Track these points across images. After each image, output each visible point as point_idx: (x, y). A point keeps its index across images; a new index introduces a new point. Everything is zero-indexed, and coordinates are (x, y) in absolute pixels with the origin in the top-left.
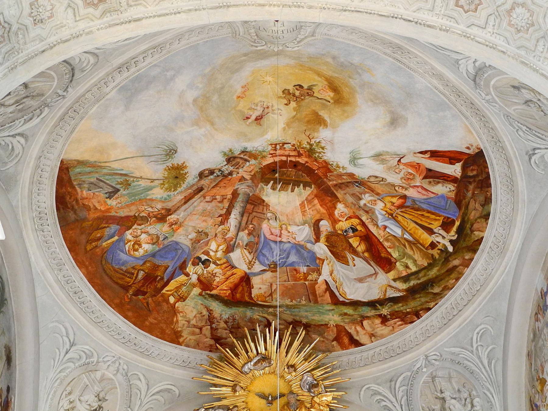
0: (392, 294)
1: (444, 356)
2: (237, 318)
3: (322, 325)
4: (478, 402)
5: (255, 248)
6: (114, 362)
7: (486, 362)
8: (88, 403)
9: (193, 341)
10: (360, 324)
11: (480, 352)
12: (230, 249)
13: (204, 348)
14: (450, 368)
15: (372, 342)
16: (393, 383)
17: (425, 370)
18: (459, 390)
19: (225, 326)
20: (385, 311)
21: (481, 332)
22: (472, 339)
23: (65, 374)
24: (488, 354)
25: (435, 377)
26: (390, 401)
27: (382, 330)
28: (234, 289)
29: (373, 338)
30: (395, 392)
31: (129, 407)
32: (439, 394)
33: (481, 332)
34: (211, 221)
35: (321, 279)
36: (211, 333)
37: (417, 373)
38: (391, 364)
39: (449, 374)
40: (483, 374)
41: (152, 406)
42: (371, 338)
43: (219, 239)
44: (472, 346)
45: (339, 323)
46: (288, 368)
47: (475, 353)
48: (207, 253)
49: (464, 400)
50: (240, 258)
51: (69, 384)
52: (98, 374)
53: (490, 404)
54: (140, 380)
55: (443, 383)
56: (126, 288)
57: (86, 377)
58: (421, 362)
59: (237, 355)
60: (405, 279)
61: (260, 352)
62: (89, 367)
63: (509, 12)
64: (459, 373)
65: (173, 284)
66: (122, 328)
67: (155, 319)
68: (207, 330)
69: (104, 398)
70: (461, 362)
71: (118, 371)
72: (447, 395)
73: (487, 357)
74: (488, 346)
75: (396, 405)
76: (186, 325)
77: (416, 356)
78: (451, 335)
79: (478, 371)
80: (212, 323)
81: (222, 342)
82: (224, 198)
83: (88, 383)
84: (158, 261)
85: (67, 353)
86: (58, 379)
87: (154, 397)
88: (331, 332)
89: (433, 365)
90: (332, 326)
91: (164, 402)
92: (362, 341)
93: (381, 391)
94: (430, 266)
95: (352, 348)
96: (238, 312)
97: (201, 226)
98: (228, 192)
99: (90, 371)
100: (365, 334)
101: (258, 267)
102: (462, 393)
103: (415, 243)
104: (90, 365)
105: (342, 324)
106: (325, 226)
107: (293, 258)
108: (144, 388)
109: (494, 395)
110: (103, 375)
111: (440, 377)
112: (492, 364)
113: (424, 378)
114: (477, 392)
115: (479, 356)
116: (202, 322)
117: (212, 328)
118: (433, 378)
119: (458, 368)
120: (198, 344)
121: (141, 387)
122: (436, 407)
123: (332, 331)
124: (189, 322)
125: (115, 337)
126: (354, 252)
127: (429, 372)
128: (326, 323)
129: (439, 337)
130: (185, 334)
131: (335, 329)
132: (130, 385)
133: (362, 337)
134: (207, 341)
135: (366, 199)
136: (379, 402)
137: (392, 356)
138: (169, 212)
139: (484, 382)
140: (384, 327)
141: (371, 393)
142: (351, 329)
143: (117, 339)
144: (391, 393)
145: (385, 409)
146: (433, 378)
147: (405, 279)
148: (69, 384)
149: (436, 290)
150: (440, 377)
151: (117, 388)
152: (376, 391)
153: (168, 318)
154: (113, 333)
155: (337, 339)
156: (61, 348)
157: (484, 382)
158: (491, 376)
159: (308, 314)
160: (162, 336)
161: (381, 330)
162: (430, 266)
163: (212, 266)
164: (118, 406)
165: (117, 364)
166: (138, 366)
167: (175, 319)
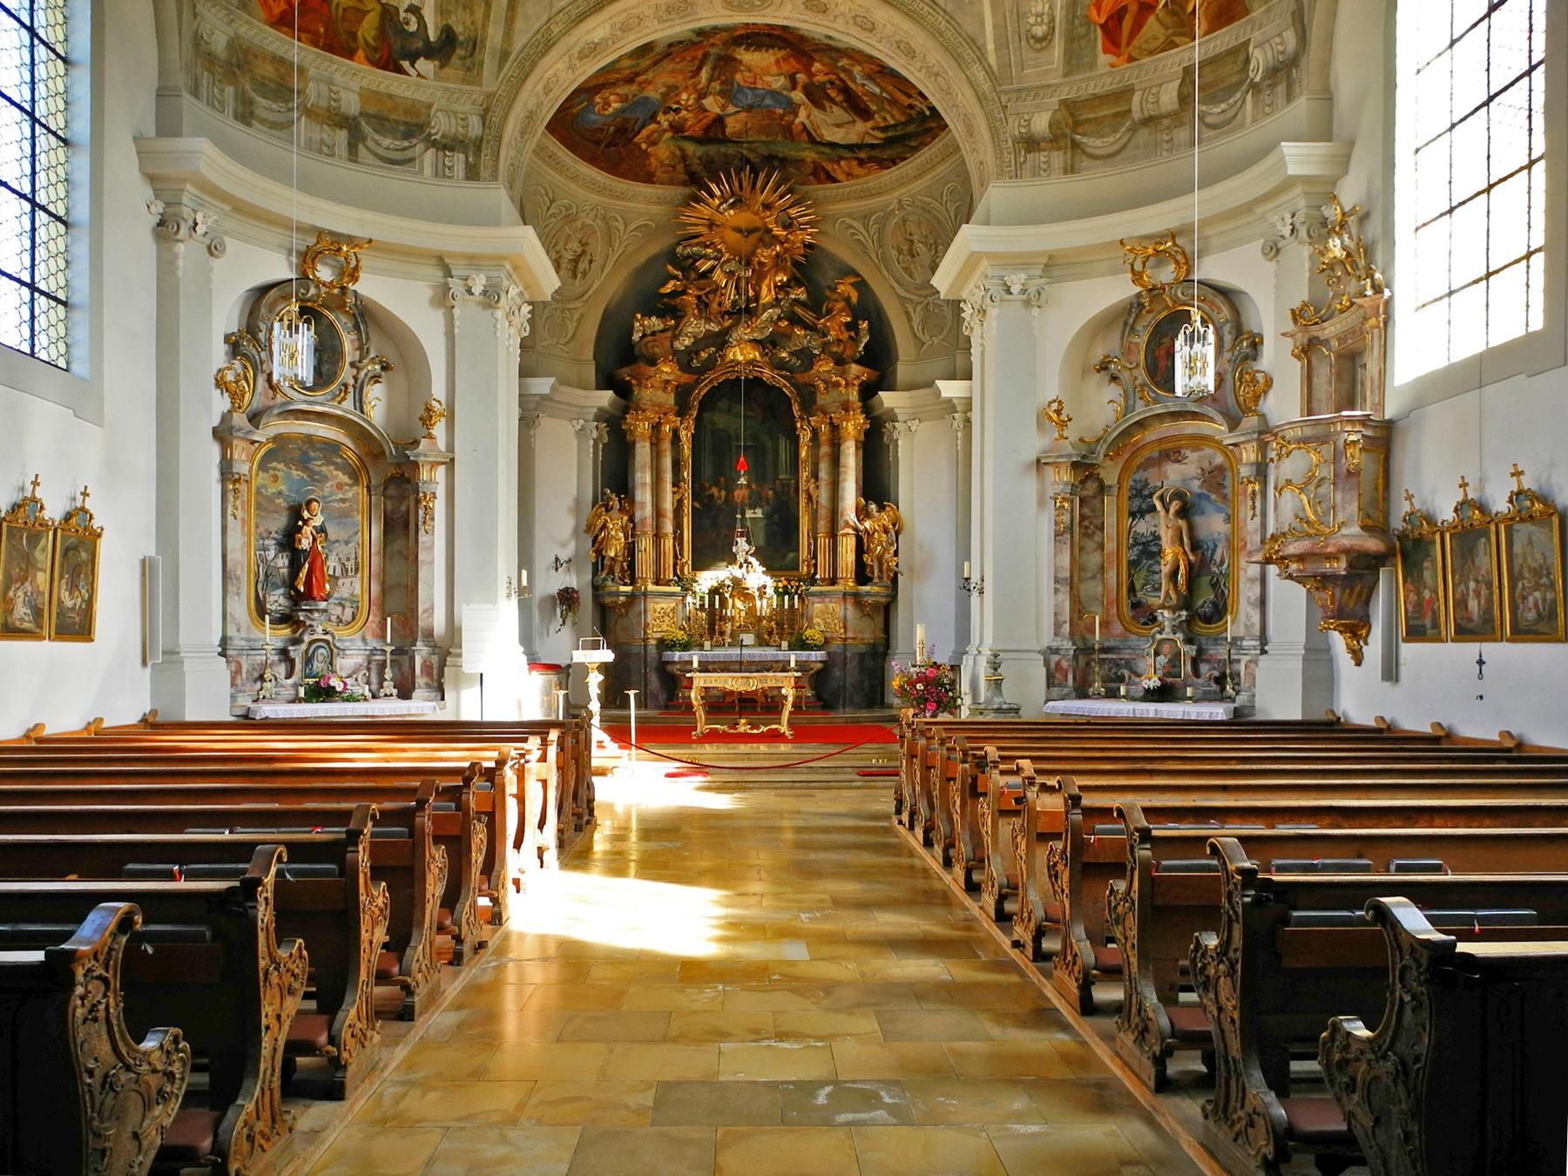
0: (869, 140)
5: (729, 93)
12: (702, 95)
20: (862, 155)
28: (707, 129)
34: (680, 77)
35: (797, 121)
43: (691, 89)
48: (678, 103)
50: (712, 104)
52: (579, 224)
56: (598, 143)
60: (884, 129)
62: (569, 219)
65: (644, 133)
68: (680, 167)
72: (915, 237)
77: (890, 198)
81: (695, 180)
82: (694, 58)
84: (627, 115)
94: (907, 123)
96: (712, 149)
97: (670, 81)
98: (700, 54)
101: (731, 109)
103: (894, 102)
106: (801, 77)
107: (768, 101)
108: (621, 227)
126: (832, 101)
130: (658, 174)
133: (840, 176)
135: (843, 62)
136: (852, 235)
138: (637, 74)
142: (829, 167)
147: (884, 129)
149: (913, 143)
155: (815, 173)
159: (784, 150)
160: (636, 178)
161: (858, 170)
162: (907, 123)
163: (684, 113)
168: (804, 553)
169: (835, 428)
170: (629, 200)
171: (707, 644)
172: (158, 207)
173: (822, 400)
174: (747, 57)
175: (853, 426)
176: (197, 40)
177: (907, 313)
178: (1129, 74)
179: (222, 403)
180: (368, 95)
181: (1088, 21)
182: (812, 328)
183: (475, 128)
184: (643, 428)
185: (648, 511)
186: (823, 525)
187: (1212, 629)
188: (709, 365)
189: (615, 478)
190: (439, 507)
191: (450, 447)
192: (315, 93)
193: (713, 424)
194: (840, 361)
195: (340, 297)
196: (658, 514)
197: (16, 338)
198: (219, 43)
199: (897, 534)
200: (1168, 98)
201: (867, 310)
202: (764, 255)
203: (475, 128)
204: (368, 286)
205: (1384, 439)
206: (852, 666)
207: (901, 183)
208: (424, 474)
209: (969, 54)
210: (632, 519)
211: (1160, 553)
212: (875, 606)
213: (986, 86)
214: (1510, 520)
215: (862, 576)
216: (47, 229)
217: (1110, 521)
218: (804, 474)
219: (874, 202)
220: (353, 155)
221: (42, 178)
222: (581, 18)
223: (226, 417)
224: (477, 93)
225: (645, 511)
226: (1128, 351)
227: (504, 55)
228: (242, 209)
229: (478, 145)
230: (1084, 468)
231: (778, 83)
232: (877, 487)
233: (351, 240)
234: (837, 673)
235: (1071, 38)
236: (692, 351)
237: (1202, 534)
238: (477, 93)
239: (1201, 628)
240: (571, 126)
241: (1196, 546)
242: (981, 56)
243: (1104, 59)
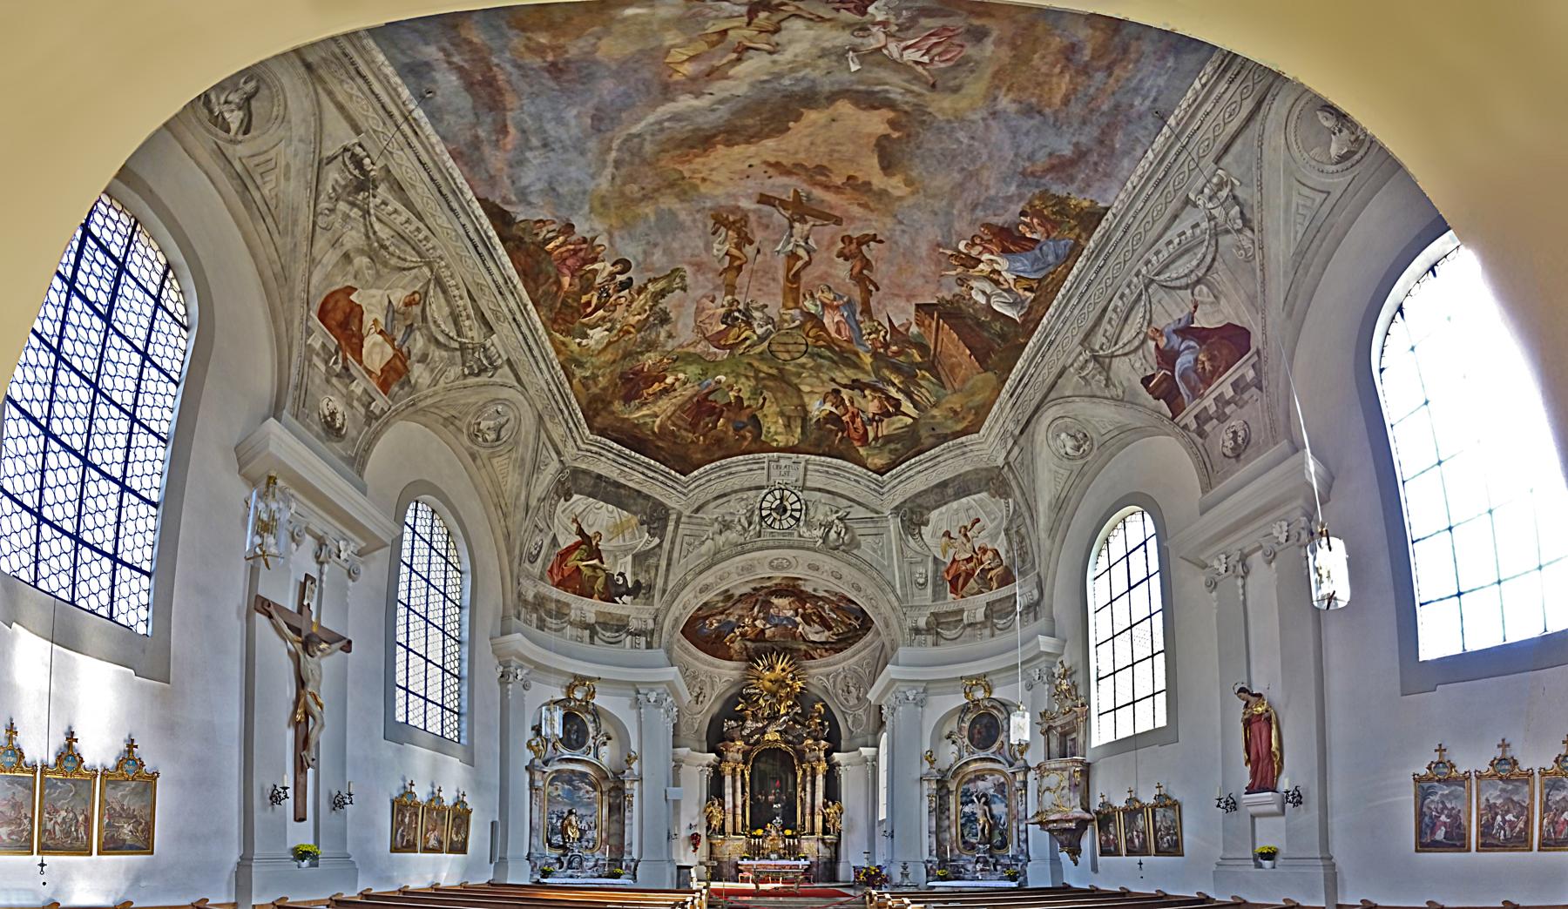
5: (766, 619)
63: (560, 847)
81: (751, 658)
103: (843, 622)
169: (813, 769)
172: (501, 669)
173: (808, 755)
174: (775, 601)
175: (822, 768)
176: (520, 594)
178: (961, 603)
179: (529, 755)
180: (598, 613)
181: (943, 578)
182: (803, 725)
183: (651, 625)
184: (728, 770)
186: (808, 811)
187: (1002, 852)
188: (758, 742)
189: (716, 789)
190: (635, 800)
191: (641, 774)
192: (574, 615)
194: (816, 739)
195: (585, 706)
196: (735, 806)
197: (19, 562)
198: (530, 597)
200: (980, 616)
201: (828, 715)
202: (783, 693)
203: (651, 625)
204: (598, 701)
205: (1087, 770)
207: (844, 660)
208: (627, 786)
209: (888, 589)
211: (977, 820)
213: (896, 604)
214: (1154, 808)
215: (826, 831)
216: (451, 681)
217: (952, 807)
220: (592, 642)
221: (448, 658)
222: (701, 573)
223: (532, 761)
224: (651, 609)
225: (729, 806)
226: (960, 729)
227: (664, 591)
228: (539, 667)
229: (652, 632)
230: (942, 783)
231: (790, 613)
233: (591, 679)
235: (935, 585)
236: (751, 735)
237: (995, 812)
238: (651, 609)
239: (997, 852)
240: (692, 630)
241: (993, 817)
242: (894, 591)
243: (950, 596)
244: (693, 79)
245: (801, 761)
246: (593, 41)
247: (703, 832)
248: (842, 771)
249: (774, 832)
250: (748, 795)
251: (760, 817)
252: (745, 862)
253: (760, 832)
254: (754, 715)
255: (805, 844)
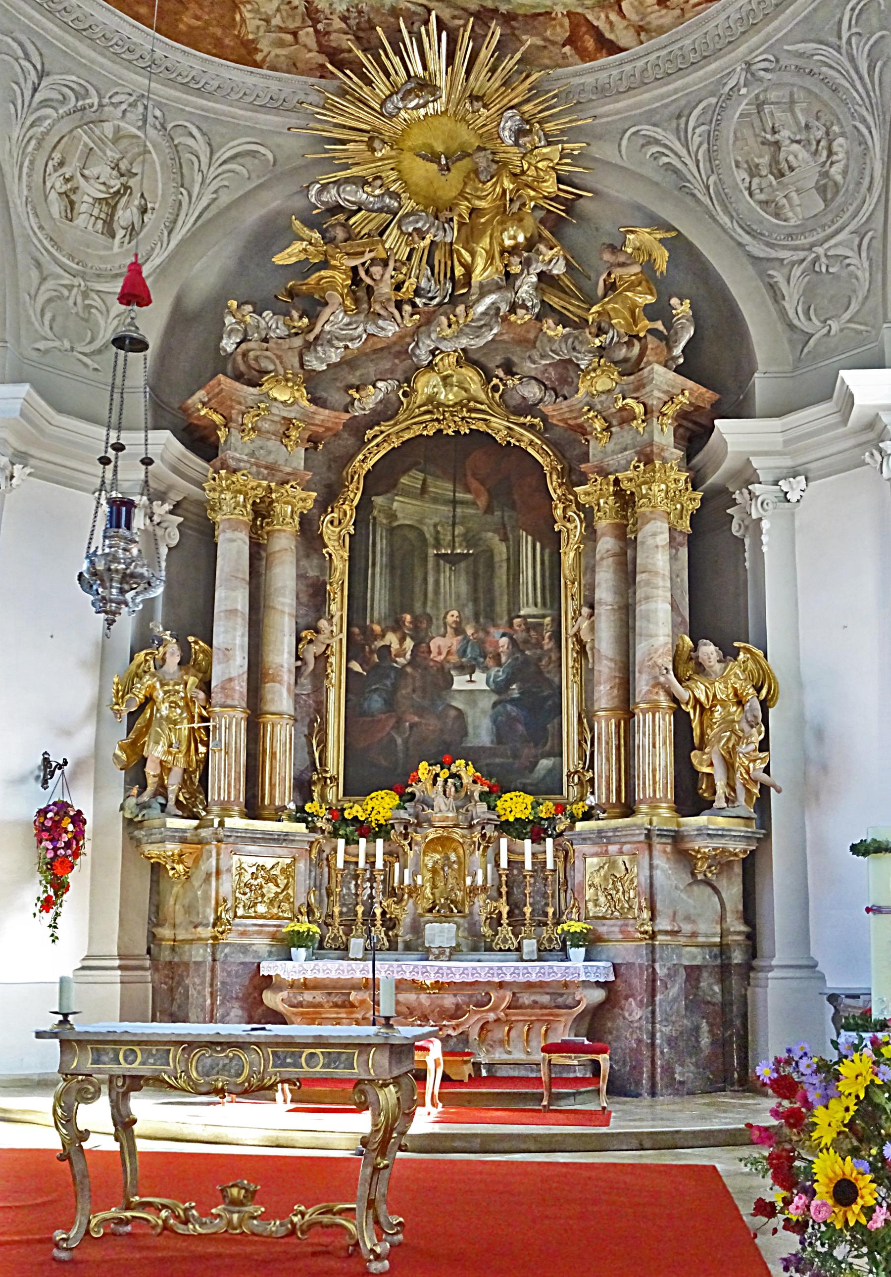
1: (783, 62)
2: (365, 9)
3: (540, 14)
4: (841, 146)
6: (133, 105)
7: (864, 67)
8: (101, 180)
9: (282, 59)
10: (617, 8)
11: (854, 46)
13: (308, 72)
14: (793, 85)
15: (642, 43)
16: (683, 120)
17: (743, 91)
18: (807, 126)
19: (344, 25)
21: (859, 7)
22: (840, 22)
23: (42, 129)
24: (870, 51)
25: (764, 103)
26: (676, 154)
27: (661, 17)
29: (643, 34)
30: (686, 137)
31: (182, 186)
32: (768, 136)
33: (859, 7)
36: (318, 42)
37: (729, 97)
38: (679, 83)
39: (792, 95)
40: (857, 91)
41: (226, 183)
42: (639, 35)
44: (840, 38)
45: (573, 10)
46: (471, 103)
47: (844, 51)
49: (814, 143)
51: (55, 147)
52: (108, 129)
53: (863, 147)
54: (194, 137)
55: (777, 114)
57: (86, 133)
58: (739, 76)
59: (369, 83)
61: (412, 74)
64: (810, 92)
66: (134, 40)
67: (198, 18)
68: (307, 35)
69: (129, 171)
70: (816, 70)
71: (145, 121)
73: (869, 55)
74: (872, 34)
75: (688, 160)
76: (262, 30)
78: (798, 19)
79: (847, 85)
80: (315, 21)
83: (92, 145)
85: (35, 90)
86: (31, 138)
87: (225, 167)
88: (558, 29)
89: (761, 80)
90: (560, 15)
91: (247, 175)
92: (622, 43)
93: (660, 138)
95: (602, 57)
99: (92, 122)
100: (626, 28)
102: (812, 131)
104: (87, 111)
105: (579, 10)
109: (873, 130)
110: (117, 129)
111: (772, 103)
112: (877, 69)
113: (742, 106)
114: (842, 127)
115: (853, 56)
116: (294, 21)
117: (317, 31)
118: (760, 106)
119: (808, 82)
120: (294, 64)
121: (197, 148)
122: (761, 160)
123: (562, 26)
124: (267, 21)
125: (123, 56)
127: (753, 94)
128: (548, 10)
129: (776, 23)
130: (264, 45)
131: (566, 21)
132: (176, 146)
133: (622, 35)
134: (311, 58)
136: (655, 157)
137: (681, 69)
139: (857, 107)
140: (664, 12)
141: (642, 141)
143: (130, 61)
144: (679, 140)
145: (666, 170)
146: (760, 106)
148: (55, 147)
150: (772, 103)
151: (150, 152)
152: (650, 136)
153: (223, 16)
154: (118, 50)
156: (22, 81)
157: (857, 107)
158: (872, 94)
164: (160, 185)
165: (141, 109)
166: (183, 110)
167: (238, 17)
168: (571, 760)
169: (626, 501)
170: (210, 95)
171: (357, 944)
173: (599, 448)
175: (667, 498)
177: (772, 287)
185: (239, 663)
186: (605, 695)
193: (393, 516)
196: (257, 674)
199: (765, 705)
206: (672, 993)
210: (206, 686)
212: (722, 862)
215: (691, 795)
218: (569, 606)
219: (695, 79)
225: (230, 665)
232: (718, 607)
234: (635, 1011)
244: (626, 554)
245: (573, 476)
246: (513, 318)
247: (98, 802)
248: (761, 506)
249: (443, 808)
250: (334, 630)
251: (387, 740)
252: (299, 966)
253: (382, 805)
254: (360, 289)
255: (590, 866)
